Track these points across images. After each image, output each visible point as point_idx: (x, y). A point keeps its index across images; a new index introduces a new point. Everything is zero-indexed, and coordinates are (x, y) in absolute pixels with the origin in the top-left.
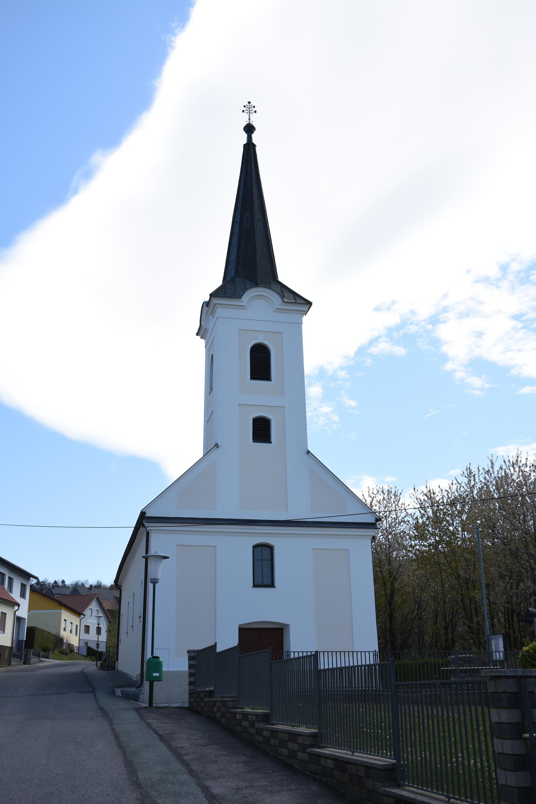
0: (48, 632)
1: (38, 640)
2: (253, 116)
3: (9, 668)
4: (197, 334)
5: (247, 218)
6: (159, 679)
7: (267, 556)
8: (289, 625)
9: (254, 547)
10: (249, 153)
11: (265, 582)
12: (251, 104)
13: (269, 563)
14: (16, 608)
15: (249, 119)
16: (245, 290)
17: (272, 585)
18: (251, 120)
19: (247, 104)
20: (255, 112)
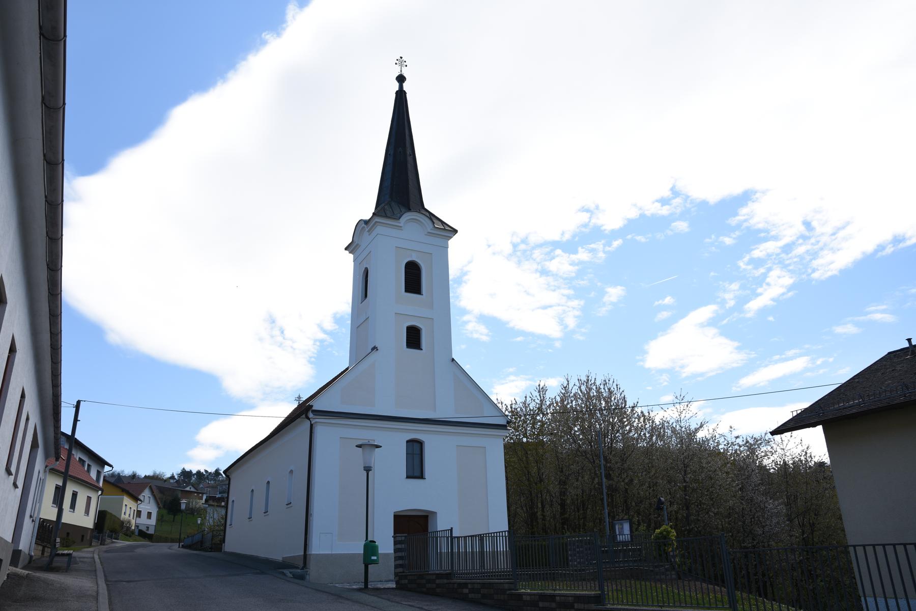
1: (108, 524)
2: (404, 69)
4: (346, 249)
6: (375, 562)
8: (435, 513)
9: (407, 442)
10: (401, 99)
11: (415, 475)
17: (421, 477)
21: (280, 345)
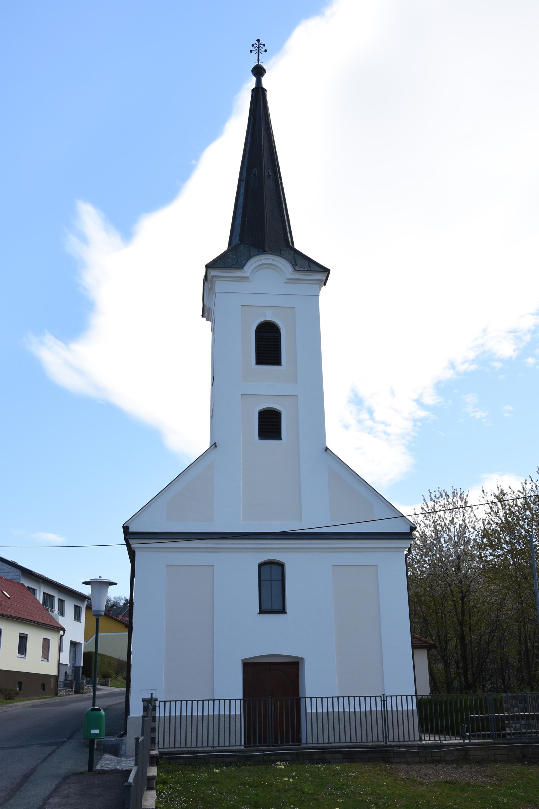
0: (111, 657)
2: (262, 56)
3: (57, 699)
5: (254, 175)
7: (276, 575)
9: (261, 565)
10: (259, 97)
12: (260, 42)
13: (280, 583)
14: (62, 633)
15: (259, 60)
16: (250, 257)
17: (283, 611)
18: (260, 61)
19: (256, 42)
20: (266, 51)
21: (371, 431)
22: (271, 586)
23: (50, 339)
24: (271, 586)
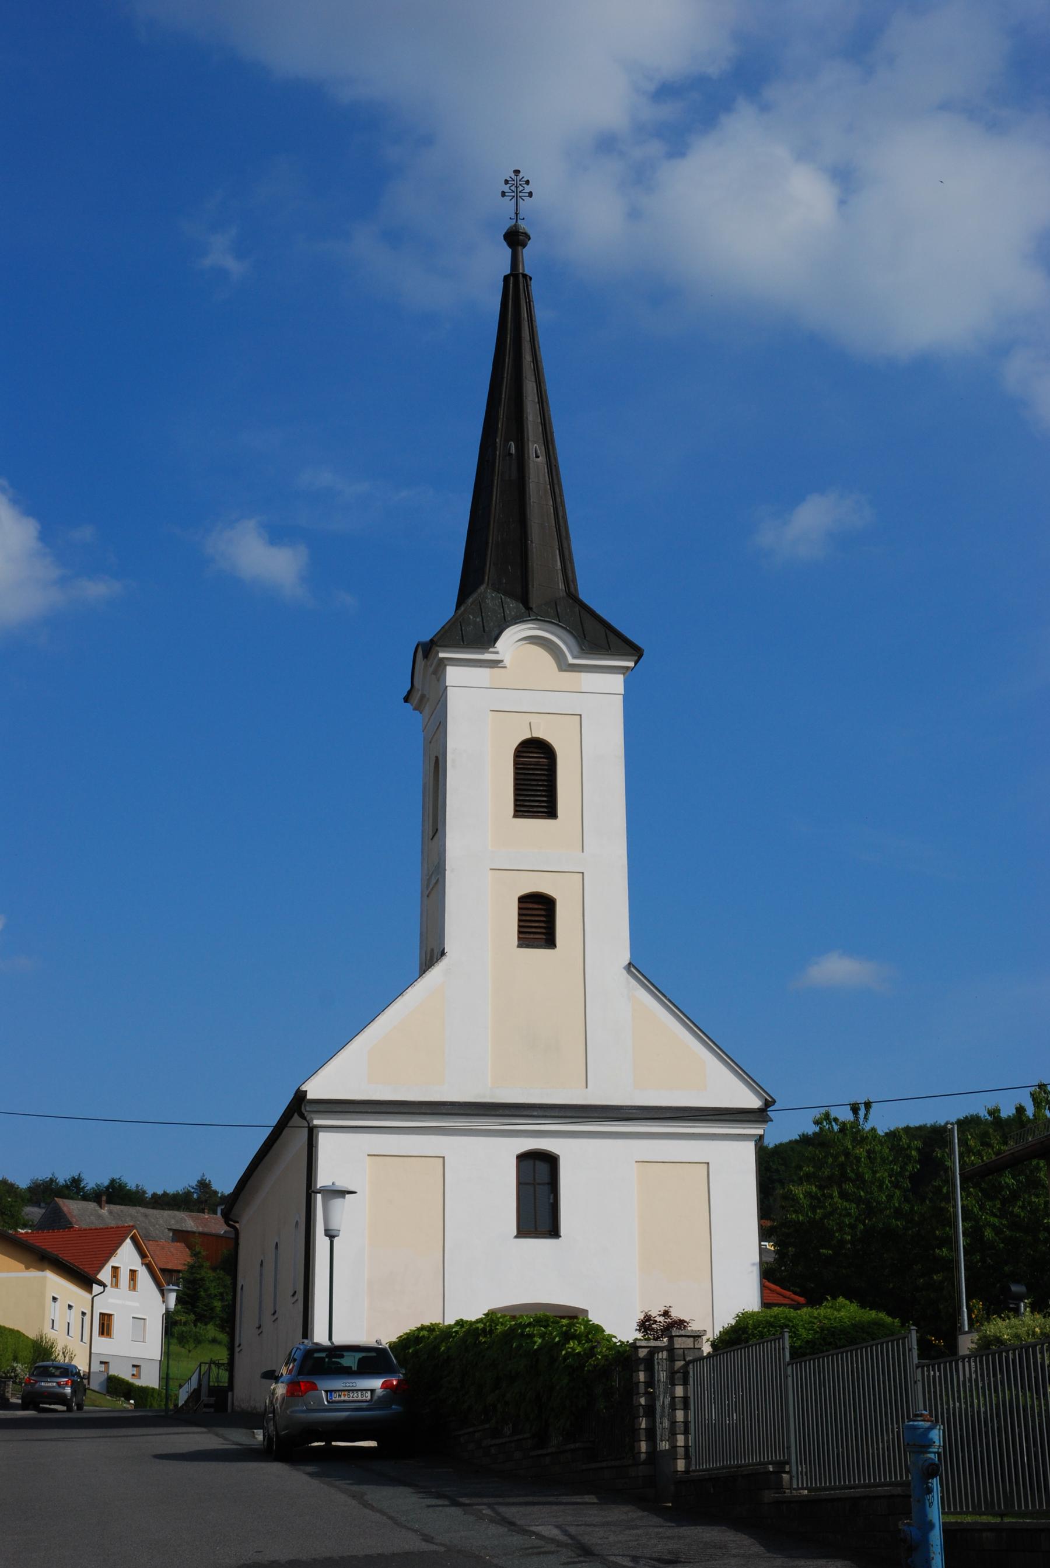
9: (522, 900)
20: (530, 194)
22: (260, 1302)
23: (810, 1133)
24: (260, 1302)
